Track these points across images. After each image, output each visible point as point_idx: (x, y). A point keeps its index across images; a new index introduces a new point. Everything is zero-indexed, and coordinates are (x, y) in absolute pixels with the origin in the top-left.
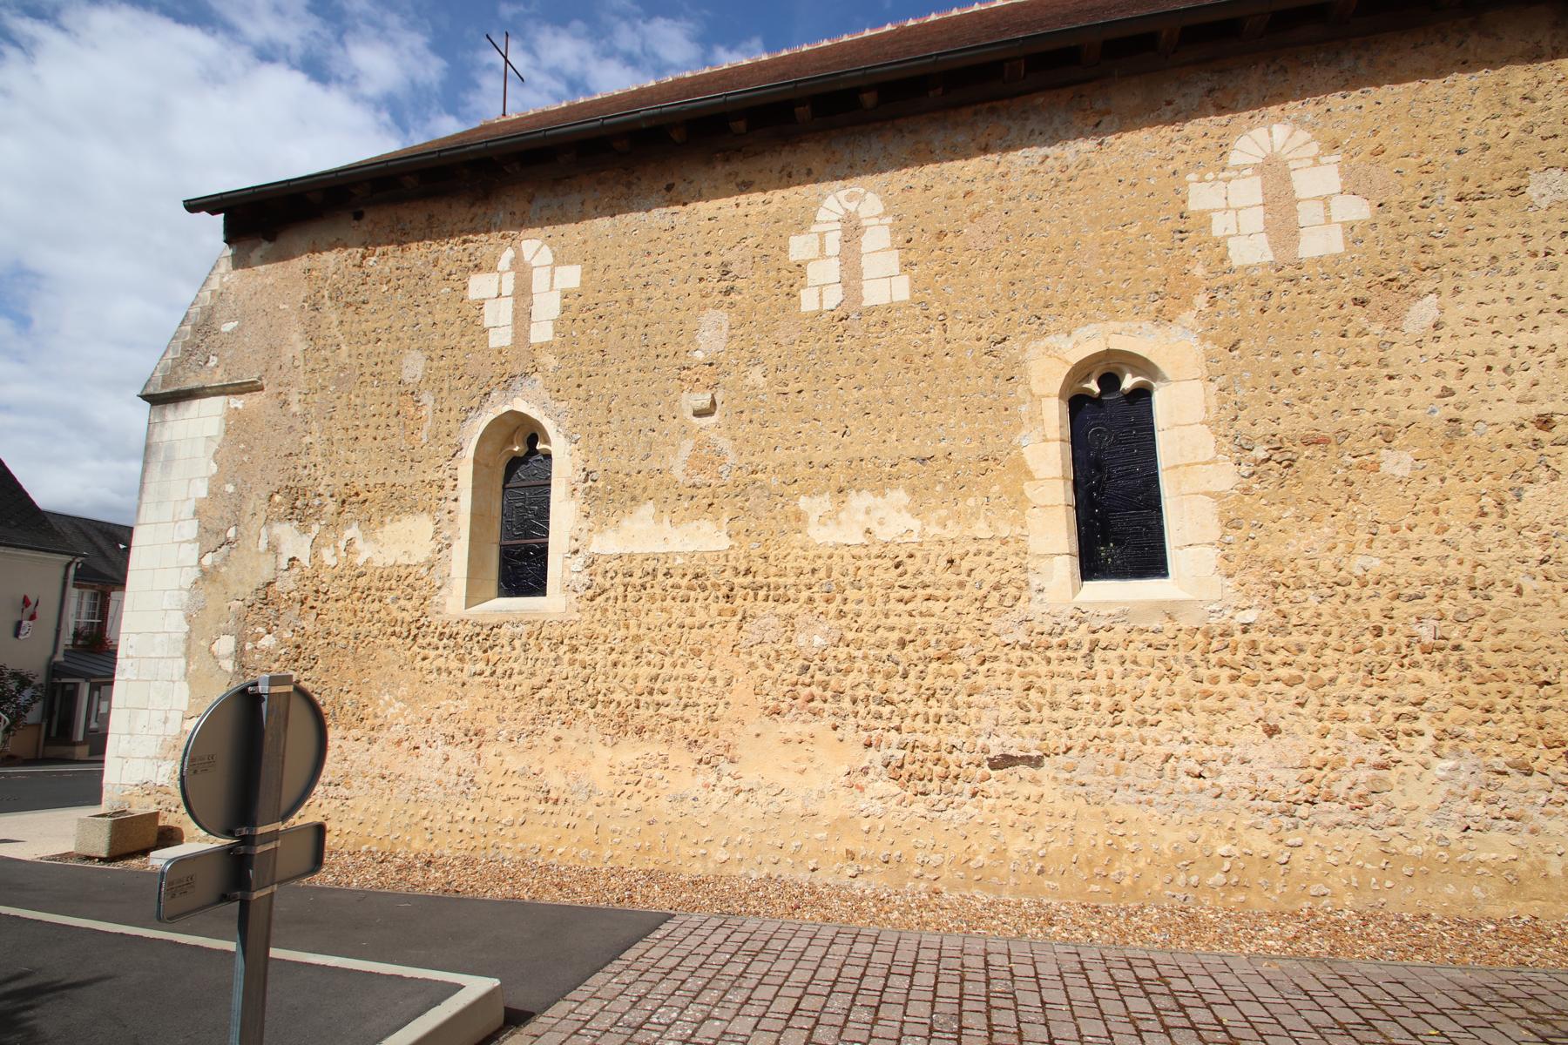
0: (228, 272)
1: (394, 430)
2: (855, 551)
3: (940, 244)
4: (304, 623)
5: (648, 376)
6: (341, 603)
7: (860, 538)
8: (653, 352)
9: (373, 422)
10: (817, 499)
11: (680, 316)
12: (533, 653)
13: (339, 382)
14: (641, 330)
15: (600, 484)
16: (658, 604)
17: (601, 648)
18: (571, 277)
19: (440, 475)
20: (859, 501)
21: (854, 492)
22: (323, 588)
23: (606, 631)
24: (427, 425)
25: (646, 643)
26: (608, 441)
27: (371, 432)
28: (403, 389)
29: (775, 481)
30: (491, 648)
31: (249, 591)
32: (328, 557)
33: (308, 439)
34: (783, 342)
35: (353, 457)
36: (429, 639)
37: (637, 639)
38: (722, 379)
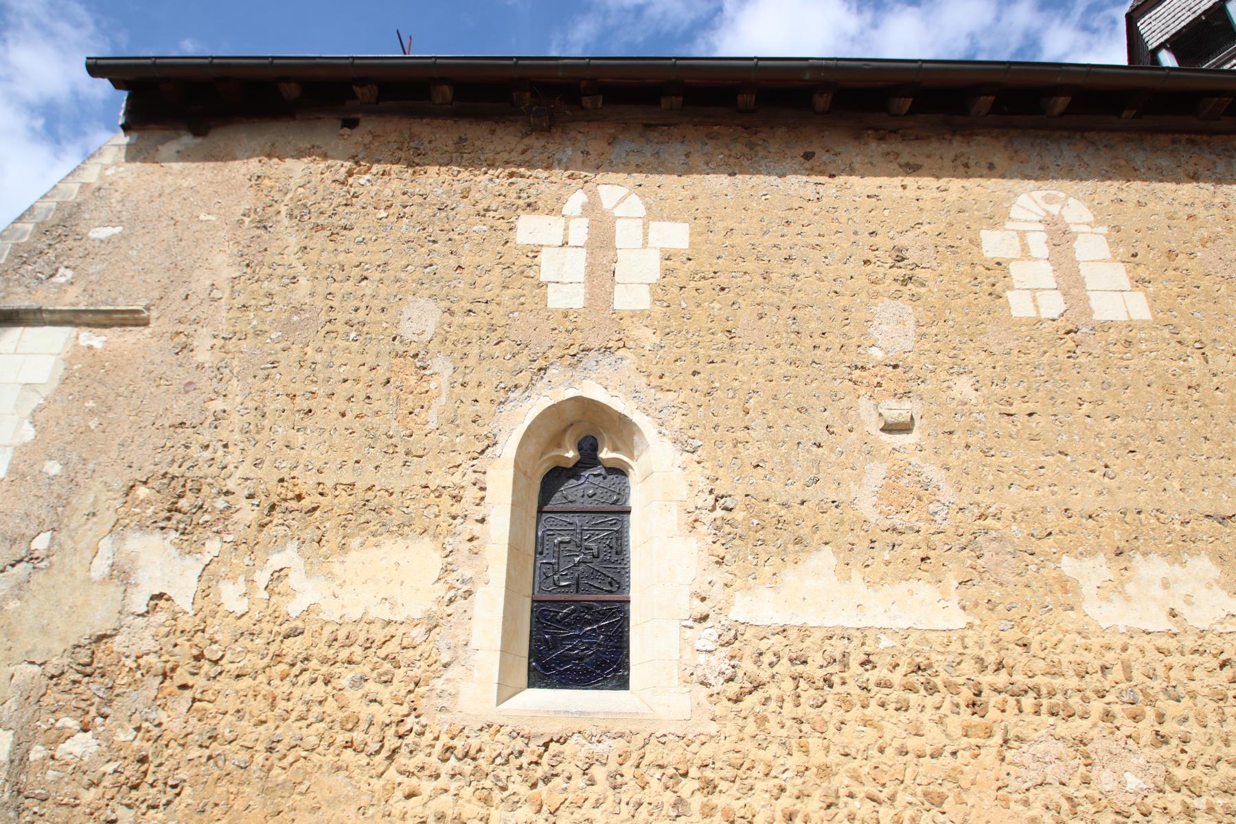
0: (116, 164)
1: (376, 405)
2: (1163, 642)
3: (1174, 264)
4: (162, 716)
5: (803, 372)
6: (245, 683)
7: (1166, 624)
8: (809, 342)
9: (343, 390)
10: (1088, 563)
11: (844, 301)
12: (630, 791)
13: (288, 328)
14: (787, 312)
15: (739, 515)
16: (857, 712)
17: (759, 785)
18: (677, 235)
19: (457, 478)
20: (1150, 568)
21: (1138, 556)
22: (212, 652)
23: (767, 755)
24: (436, 406)
25: (841, 781)
26: (749, 454)
27: (337, 404)
28: (401, 349)
29: (1017, 532)
30: (546, 780)
31: (58, 647)
32: (231, 596)
33: (219, 405)
34: (994, 349)
35: (300, 438)
36: (419, 758)
37: (825, 771)
38: (912, 385)
